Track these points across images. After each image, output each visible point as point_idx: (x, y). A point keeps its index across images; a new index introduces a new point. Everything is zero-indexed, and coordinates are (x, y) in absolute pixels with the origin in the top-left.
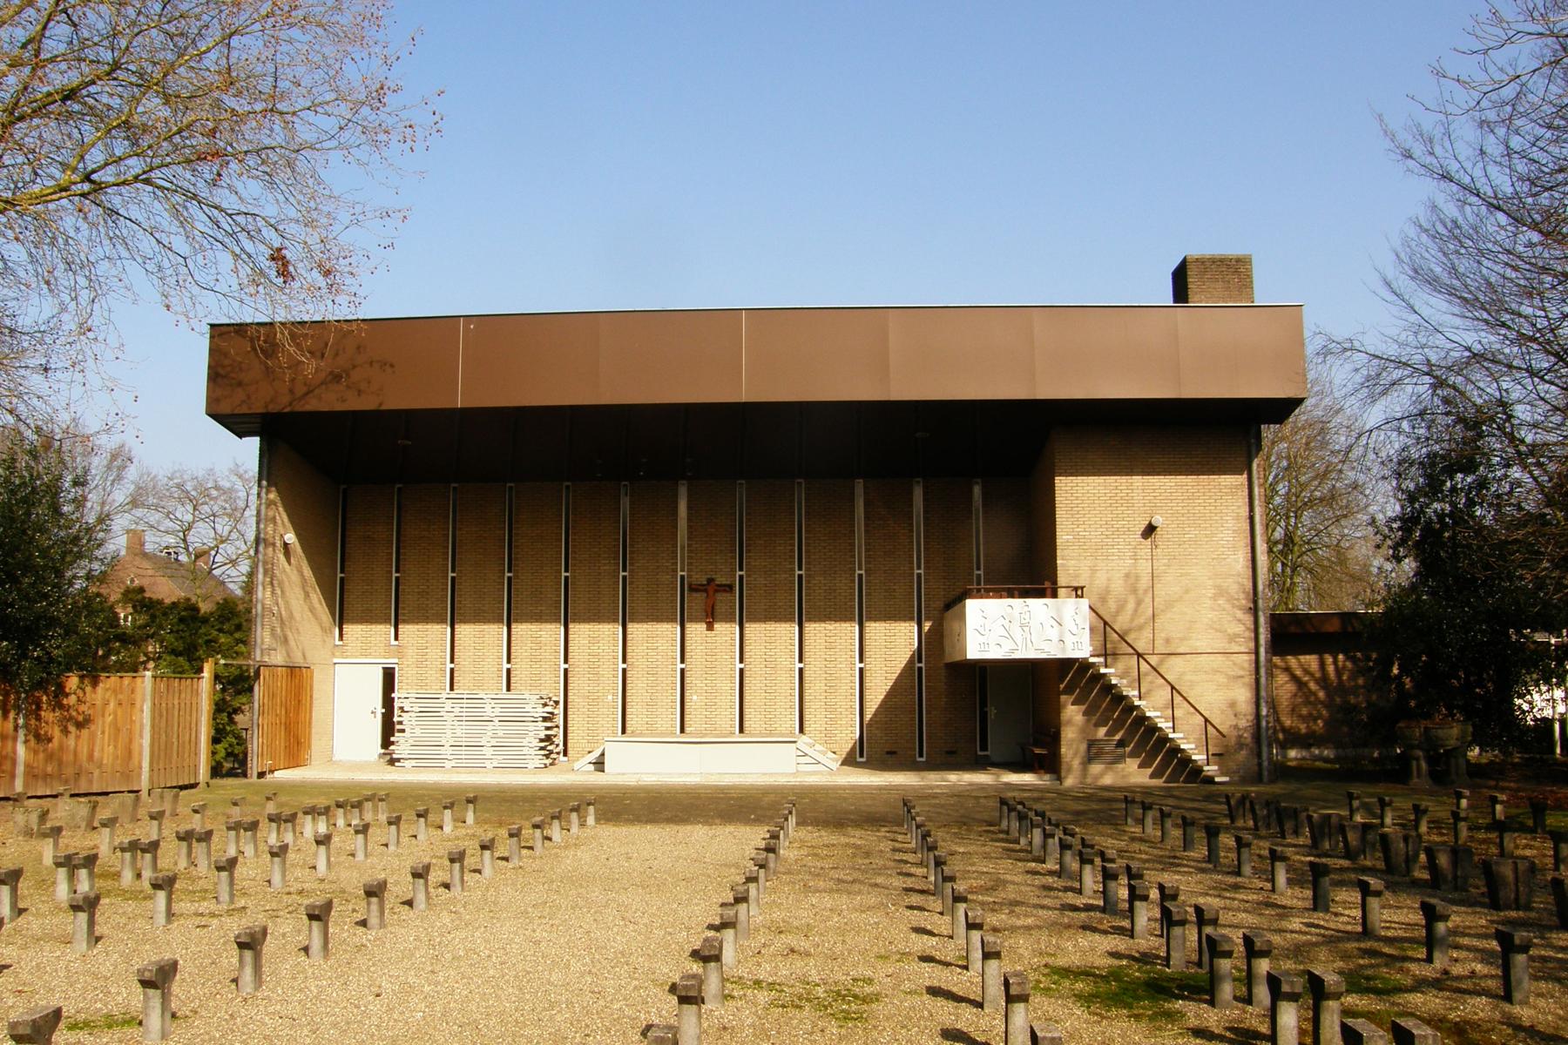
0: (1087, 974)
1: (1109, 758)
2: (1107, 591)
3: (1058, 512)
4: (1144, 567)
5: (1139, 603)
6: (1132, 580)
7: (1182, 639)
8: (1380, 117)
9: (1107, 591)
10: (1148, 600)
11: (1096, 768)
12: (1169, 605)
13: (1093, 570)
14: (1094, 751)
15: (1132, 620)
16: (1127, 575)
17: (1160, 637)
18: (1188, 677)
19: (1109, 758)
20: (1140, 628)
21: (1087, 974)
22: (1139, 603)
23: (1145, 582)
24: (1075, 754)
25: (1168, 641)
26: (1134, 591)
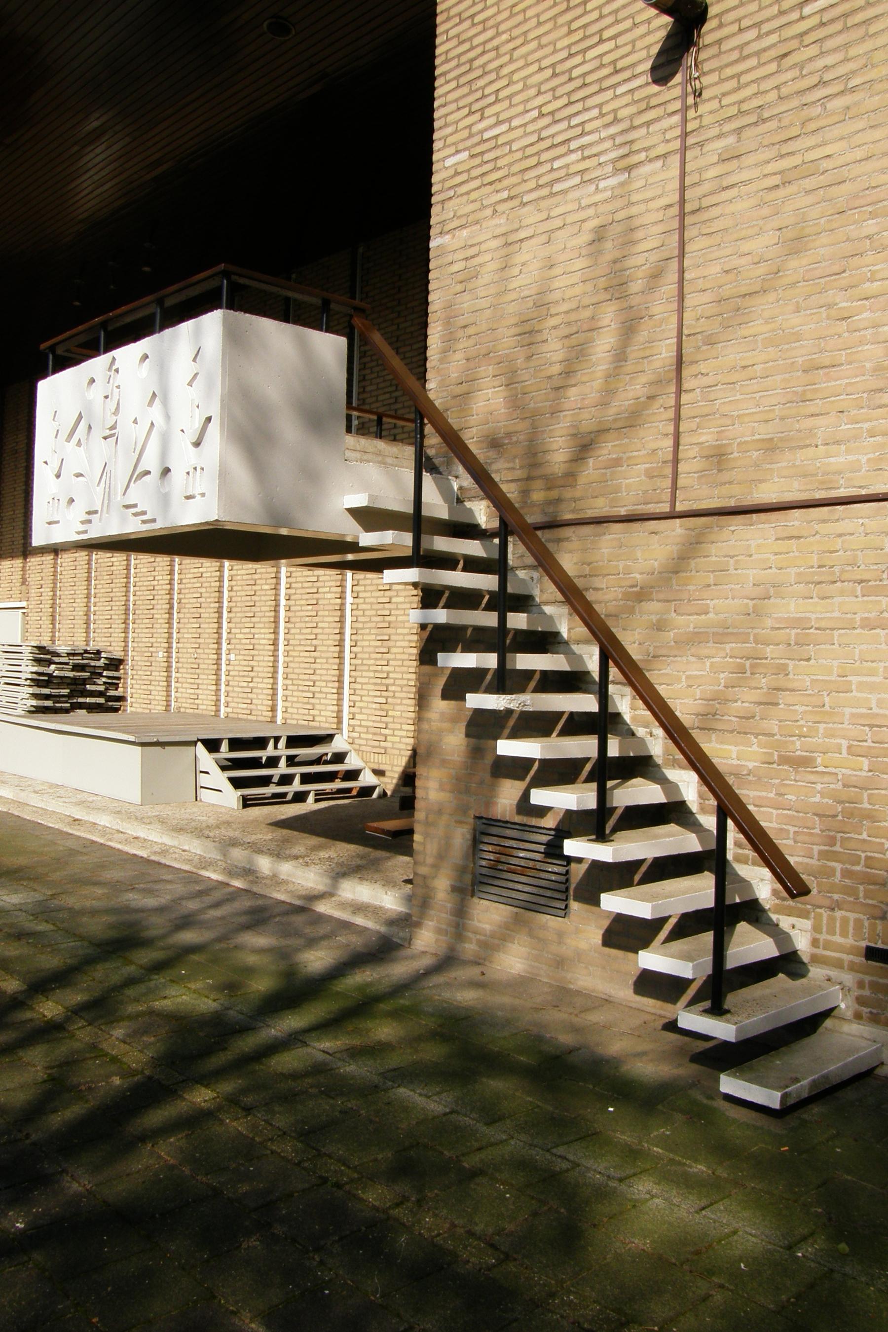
0: (568, 373)
1: (523, 887)
2: (541, 304)
3: (442, 89)
4: (657, 182)
5: (629, 328)
6: (610, 250)
7: (770, 447)
8: (787, 227)
9: (541, 304)
10: (661, 306)
11: (488, 914)
12: (734, 308)
13: (510, 243)
14: (488, 854)
15: (609, 392)
16: (599, 236)
17: (699, 438)
18: (790, 607)
19: (523, 887)
20: (632, 420)
21: (568, 373)
22: (629, 328)
23: (652, 242)
24: (441, 857)
25: (718, 457)
26: (617, 286)
